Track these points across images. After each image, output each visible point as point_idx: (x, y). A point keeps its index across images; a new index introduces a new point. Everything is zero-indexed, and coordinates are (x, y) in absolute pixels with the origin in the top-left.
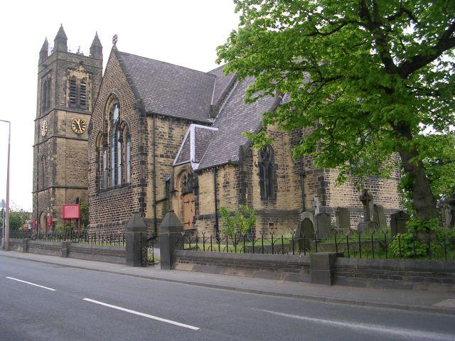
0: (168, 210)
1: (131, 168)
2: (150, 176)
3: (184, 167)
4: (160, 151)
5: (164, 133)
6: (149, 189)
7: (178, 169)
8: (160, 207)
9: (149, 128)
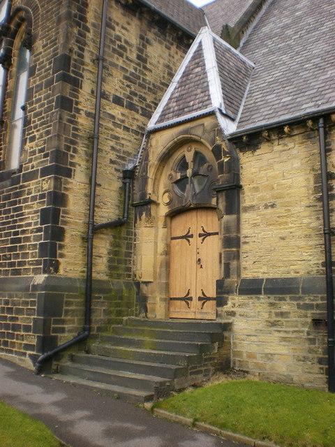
0: (122, 257)
1: (27, 122)
2: (81, 149)
3: (186, 132)
4: (114, 85)
5: (127, 42)
6: (77, 185)
7: (161, 143)
8: (103, 246)
9: (90, 16)
